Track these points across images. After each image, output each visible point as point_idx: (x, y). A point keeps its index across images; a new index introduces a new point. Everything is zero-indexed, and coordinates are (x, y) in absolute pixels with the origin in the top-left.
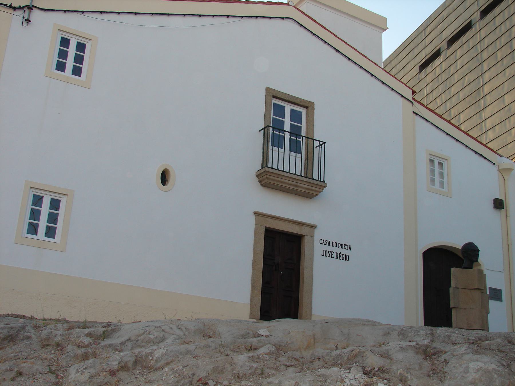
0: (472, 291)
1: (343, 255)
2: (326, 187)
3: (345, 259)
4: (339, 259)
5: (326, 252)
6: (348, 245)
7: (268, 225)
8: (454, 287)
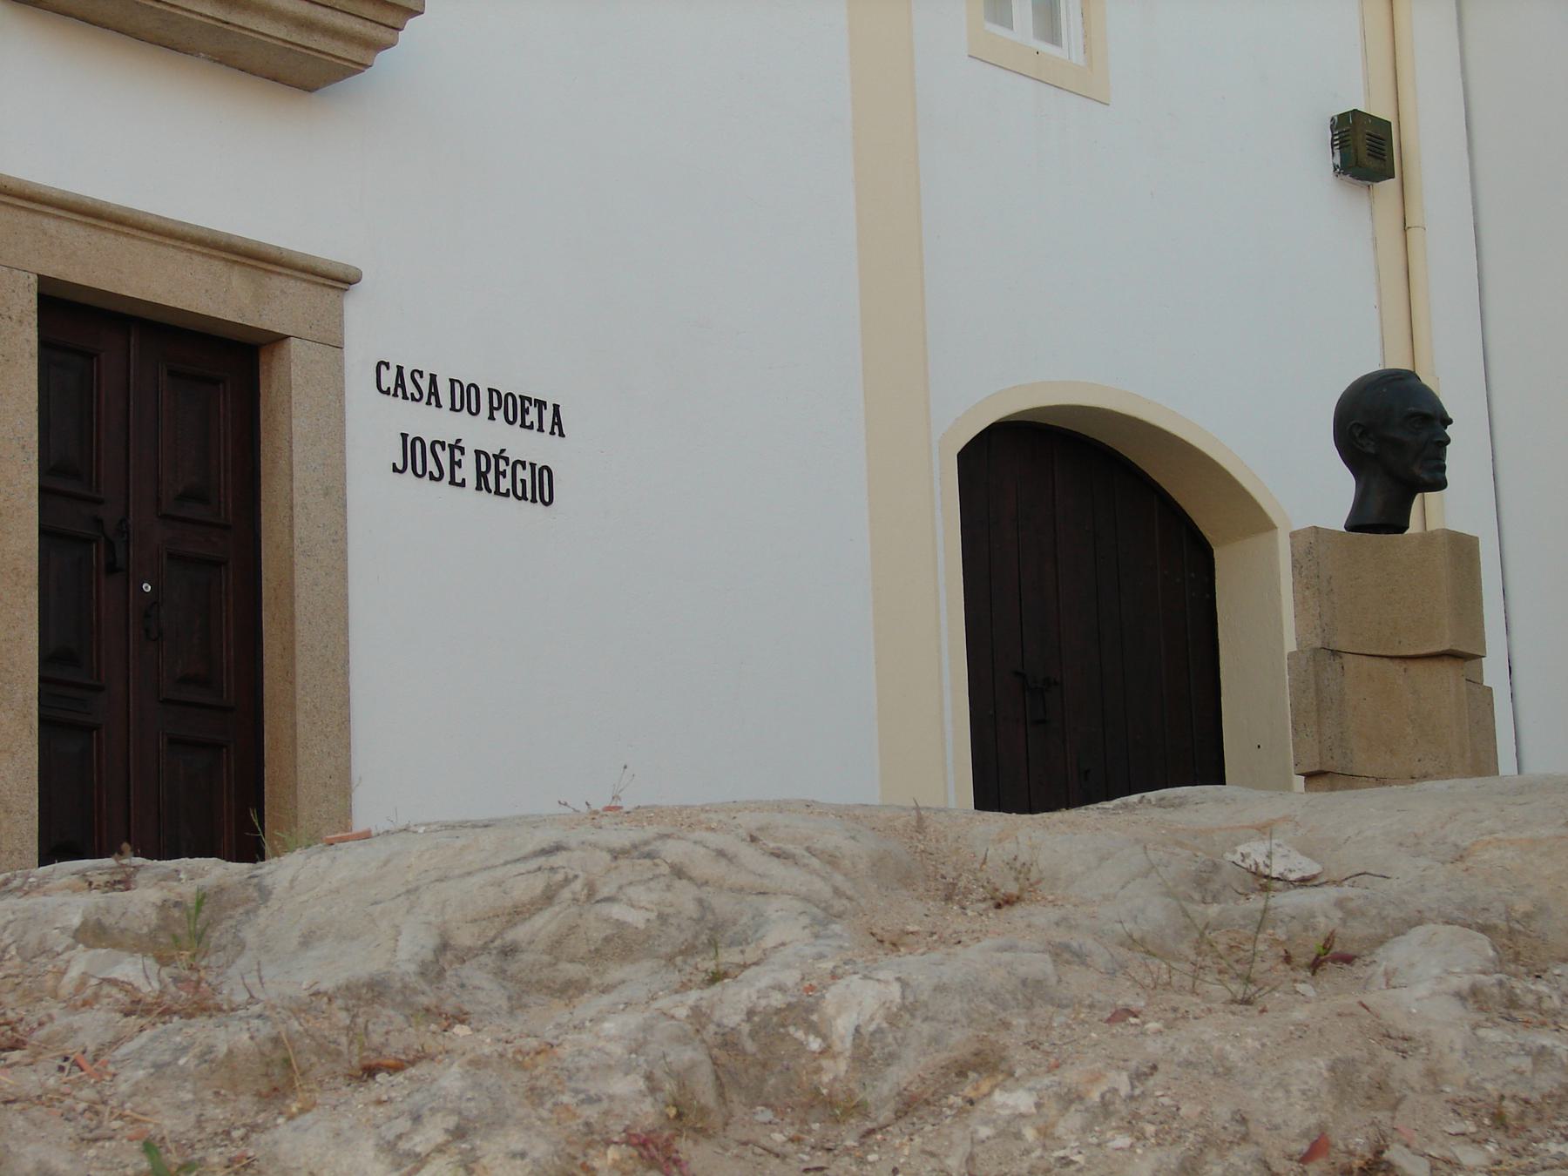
0: (1416, 668)
1: (519, 467)
2: (422, 13)
3: (529, 495)
4: (497, 492)
5: (418, 444)
6: (545, 403)
7: (58, 269)
8: (1318, 644)
